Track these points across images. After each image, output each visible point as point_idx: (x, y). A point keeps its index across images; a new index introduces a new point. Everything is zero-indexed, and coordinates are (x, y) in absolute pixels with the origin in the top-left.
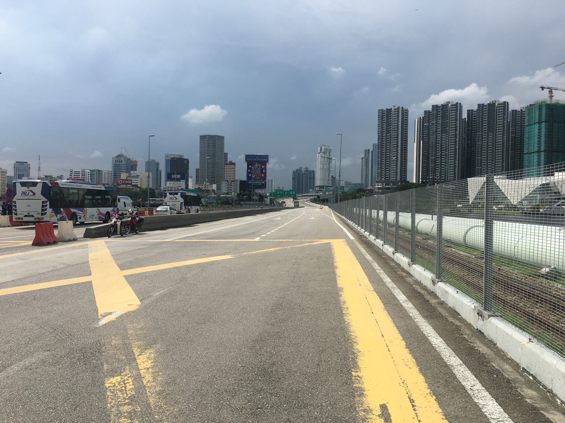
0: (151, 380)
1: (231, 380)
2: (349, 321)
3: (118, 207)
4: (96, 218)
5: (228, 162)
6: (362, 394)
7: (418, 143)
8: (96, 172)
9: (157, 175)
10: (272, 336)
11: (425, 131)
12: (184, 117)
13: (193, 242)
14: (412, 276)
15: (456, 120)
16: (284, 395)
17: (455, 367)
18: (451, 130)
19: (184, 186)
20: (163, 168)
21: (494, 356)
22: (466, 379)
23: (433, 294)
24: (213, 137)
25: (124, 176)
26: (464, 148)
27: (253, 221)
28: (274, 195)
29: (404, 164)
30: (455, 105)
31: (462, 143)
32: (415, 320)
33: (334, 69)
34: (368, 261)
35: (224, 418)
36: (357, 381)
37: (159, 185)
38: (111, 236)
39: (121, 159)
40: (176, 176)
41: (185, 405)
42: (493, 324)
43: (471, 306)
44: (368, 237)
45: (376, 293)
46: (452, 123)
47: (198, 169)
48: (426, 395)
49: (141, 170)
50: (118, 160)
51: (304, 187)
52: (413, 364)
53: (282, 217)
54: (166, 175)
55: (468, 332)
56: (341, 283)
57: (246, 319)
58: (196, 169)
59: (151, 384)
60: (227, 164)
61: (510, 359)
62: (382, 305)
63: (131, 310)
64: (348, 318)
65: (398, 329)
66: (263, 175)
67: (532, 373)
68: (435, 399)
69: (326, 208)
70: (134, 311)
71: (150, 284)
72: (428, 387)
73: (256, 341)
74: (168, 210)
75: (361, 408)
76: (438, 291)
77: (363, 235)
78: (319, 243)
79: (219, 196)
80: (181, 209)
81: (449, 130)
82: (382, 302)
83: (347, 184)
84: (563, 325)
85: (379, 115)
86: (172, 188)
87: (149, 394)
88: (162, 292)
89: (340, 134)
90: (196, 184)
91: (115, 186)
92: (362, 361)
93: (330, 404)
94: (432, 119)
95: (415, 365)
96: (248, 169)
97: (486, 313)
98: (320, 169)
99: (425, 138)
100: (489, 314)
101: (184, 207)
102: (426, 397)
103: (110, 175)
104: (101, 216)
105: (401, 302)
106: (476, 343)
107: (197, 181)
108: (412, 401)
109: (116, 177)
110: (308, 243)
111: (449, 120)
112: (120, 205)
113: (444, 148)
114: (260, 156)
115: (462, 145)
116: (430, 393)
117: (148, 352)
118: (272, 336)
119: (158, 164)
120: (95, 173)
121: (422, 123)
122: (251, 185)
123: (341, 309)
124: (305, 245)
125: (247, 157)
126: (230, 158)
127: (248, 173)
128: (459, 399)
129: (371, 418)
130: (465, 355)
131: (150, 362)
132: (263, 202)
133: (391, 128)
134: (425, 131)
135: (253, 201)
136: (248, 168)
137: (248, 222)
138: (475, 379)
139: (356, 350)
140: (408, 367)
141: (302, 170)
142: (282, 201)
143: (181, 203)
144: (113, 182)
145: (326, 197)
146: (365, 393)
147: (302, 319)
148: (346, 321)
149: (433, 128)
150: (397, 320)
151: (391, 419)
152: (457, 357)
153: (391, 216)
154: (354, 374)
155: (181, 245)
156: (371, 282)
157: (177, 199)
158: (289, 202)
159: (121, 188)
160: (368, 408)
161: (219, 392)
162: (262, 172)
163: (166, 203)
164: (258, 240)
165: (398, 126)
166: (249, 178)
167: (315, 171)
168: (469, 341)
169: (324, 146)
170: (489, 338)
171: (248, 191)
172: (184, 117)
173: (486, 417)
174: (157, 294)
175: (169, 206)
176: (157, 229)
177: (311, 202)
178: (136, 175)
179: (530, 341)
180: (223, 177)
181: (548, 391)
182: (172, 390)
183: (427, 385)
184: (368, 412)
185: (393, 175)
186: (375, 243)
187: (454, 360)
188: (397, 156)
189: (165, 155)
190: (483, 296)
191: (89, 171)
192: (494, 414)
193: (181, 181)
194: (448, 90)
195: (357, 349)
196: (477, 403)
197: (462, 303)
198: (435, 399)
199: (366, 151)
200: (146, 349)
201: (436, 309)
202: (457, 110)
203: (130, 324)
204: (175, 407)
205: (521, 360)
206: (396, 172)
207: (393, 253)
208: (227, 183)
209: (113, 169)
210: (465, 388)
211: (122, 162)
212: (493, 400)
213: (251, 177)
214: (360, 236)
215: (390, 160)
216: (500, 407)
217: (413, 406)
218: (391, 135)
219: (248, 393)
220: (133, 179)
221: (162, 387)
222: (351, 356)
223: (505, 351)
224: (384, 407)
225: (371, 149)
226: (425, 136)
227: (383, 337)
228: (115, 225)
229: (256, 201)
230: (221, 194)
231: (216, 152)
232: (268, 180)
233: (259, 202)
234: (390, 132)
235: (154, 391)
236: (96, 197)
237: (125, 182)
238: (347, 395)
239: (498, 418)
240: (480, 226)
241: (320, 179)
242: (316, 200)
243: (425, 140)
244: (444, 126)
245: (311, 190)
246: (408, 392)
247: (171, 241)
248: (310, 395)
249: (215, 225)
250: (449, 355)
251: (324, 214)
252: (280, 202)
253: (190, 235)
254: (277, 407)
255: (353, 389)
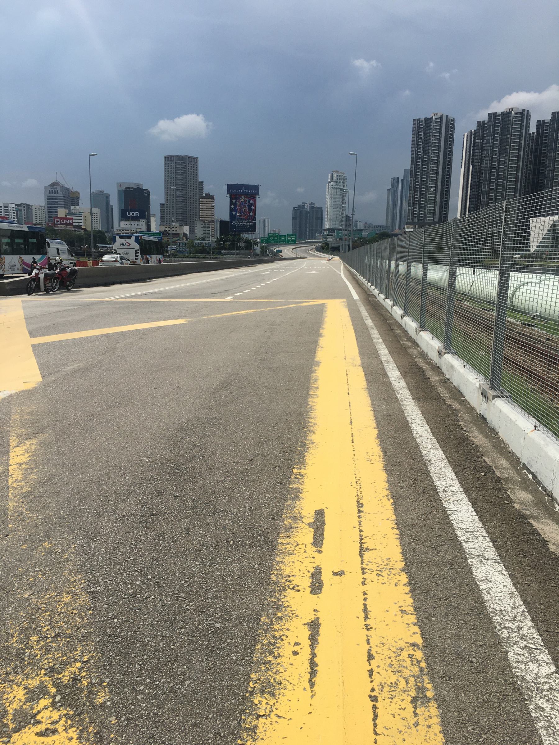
0: (19, 479)
1: (128, 479)
2: (313, 404)
3: (49, 254)
4: (18, 269)
5: (204, 195)
6: (298, 496)
7: (466, 169)
8: (24, 207)
9: (107, 212)
10: (203, 424)
11: (477, 151)
12: (154, 131)
13: (141, 302)
14: (418, 346)
15: (521, 135)
16: (192, 498)
17: (434, 462)
18: (513, 150)
19: (144, 228)
20: (114, 202)
21: (491, 448)
22: (442, 477)
23: (437, 370)
24: (182, 159)
25: (62, 213)
26: (529, 176)
27: (232, 275)
28: (266, 241)
29: (446, 198)
30: (520, 113)
31: (527, 168)
32: (402, 403)
33: (359, 63)
34: (366, 328)
35: (101, 527)
36: (296, 480)
37: (110, 226)
38: (32, 293)
39: (56, 188)
40: (133, 214)
41: (55, 511)
42: (497, 407)
43: (475, 384)
44: (377, 296)
45: (362, 369)
46: (514, 139)
47: (163, 205)
48: (382, 498)
49: (85, 204)
50: (52, 191)
51: (308, 230)
52: (378, 459)
53: (272, 270)
54: (119, 213)
55: (467, 417)
56: (320, 355)
57: (177, 401)
58: (161, 204)
59: (18, 484)
60: (203, 198)
61: (510, 453)
62: (365, 383)
63: (25, 389)
64: (314, 400)
65: (374, 414)
66: (251, 213)
67: (533, 471)
68: (391, 503)
69: (337, 259)
70: (30, 391)
71: (64, 355)
72: (388, 488)
73: (180, 429)
74: (118, 259)
75: (289, 515)
76: (443, 365)
77: (373, 294)
78: (311, 304)
79: (192, 242)
80: (136, 259)
81: (510, 149)
82: (367, 380)
83: (367, 226)
84: (557, 406)
85: (413, 128)
86: (128, 230)
87: (11, 496)
88: (76, 366)
89: (355, 155)
90: (161, 225)
91: (51, 226)
92: (312, 457)
93: (250, 510)
94: (488, 133)
95: (381, 459)
96: (231, 205)
97: (491, 393)
98: (331, 205)
99: (476, 161)
100: (495, 394)
101: (140, 256)
102: (380, 500)
103: (43, 212)
104: (24, 266)
105: (391, 379)
106: (472, 432)
107: (162, 221)
108: (360, 505)
109: (52, 215)
110: (294, 304)
111: (511, 135)
112: (51, 252)
113: (501, 175)
114: (247, 187)
115: (527, 171)
116: (387, 496)
117: (29, 442)
118: (203, 424)
119: (107, 197)
120: (23, 208)
121: (473, 139)
122: (234, 226)
123: (308, 388)
124: (291, 306)
125: (230, 187)
126: (207, 189)
127: (231, 210)
128: (424, 503)
129: (298, 527)
130: (452, 447)
131: (27, 455)
132: (251, 251)
133: (429, 146)
134: (477, 151)
135: (238, 249)
136: (231, 204)
137: (224, 277)
138: (454, 477)
139: (309, 441)
140: (371, 462)
141: (306, 207)
142: (277, 249)
143: (136, 251)
144: (47, 221)
145: (337, 245)
146: (301, 495)
147: (252, 402)
148: (309, 405)
149: (489, 145)
150: (377, 403)
151: (324, 528)
152: (441, 450)
153: (417, 269)
154: (295, 471)
155: (123, 306)
156: (361, 354)
157: (130, 245)
158: (286, 251)
159: (58, 230)
160: (298, 515)
161: (107, 494)
162: (250, 209)
163: (116, 250)
164: (229, 300)
165: (439, 143)
166: (232, 217)
167: (323, 209)
168: (465, 429)
169: (337, 172)
170: (491, 425)
171: (231, 235)
172: (154, 131)
173: (452, 525)
174: (69, 368)
175: (119, 254)
176: (98, 285)
177: (317, 251)
178: (78, 212)
179: (535, 429)
180: (198, 216)
181: (548, 494)
182: (43, 492)
183: (387, 485)
184: (296, 519)
185: (430, 214)
186: (384, 304)
187: (435, 454)
188: (436, 187)
189: (117, 183)
190: (489, 370)
191: (14, 206)
192: (464, 523)
193: (141, 220)
194: (517, 92)
195: (311, 440)
196: (446, 508)
197: (467, 380)
198: (391, 503)
199: (393, 179)
200: (27, 439)
201: (435, 389)
202: (522, 121)
203: (18, 407)
204: (40, 513)
205: (523, 453)
206: (434, 210)
207: (401, 317)
208: (203, 224)
209: (47, 203)
210: (436, 489)
211: (58, 193)
212: (468, 504)
213: (235, 216)
214: (369, 294)
215: (426, 193)
216: (475, 514)
217: (359, 511)
218: (429, 156)
219: (145, 495)
220: (74, 218)
221: (31, 488)
222: (299, 449)
223: (507, 442)
224: (320, 514)
225: (401, 178)
226: (476, 157)
227: (351, 424)
228: (36, 279)
229: (242, 249)
230: (195, 240)
231: (187, 180)
232: (260, 221)
233: (247, 251)
234: (428, 153)
235: (20, 493)
236: (17, 241)
237: (65, 221)
238: (276, 498)
239: (468, 527)
240: (536, 283)
241: (330, 220)
242: (323, 249)
243: (476, 164)
244: (503, 143)
245: (317, 235)
246: (359, 494)
247: (111, 301)
248: (227, 498)
249: (181, 280)
250: (429, 447)
251: (330, 267)
252: (275, 251)
253: (140, 293)
254: (178, 513)
255: (288, 491)
